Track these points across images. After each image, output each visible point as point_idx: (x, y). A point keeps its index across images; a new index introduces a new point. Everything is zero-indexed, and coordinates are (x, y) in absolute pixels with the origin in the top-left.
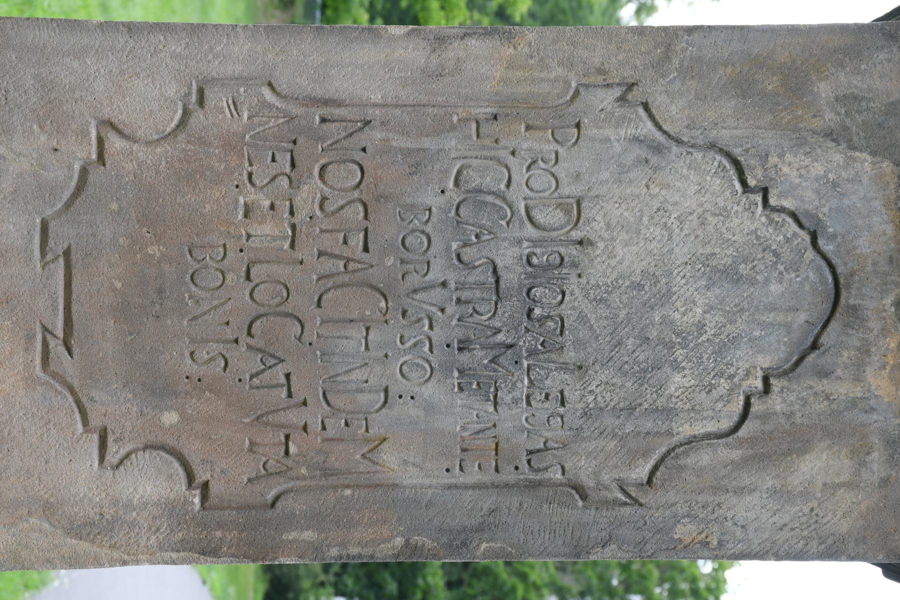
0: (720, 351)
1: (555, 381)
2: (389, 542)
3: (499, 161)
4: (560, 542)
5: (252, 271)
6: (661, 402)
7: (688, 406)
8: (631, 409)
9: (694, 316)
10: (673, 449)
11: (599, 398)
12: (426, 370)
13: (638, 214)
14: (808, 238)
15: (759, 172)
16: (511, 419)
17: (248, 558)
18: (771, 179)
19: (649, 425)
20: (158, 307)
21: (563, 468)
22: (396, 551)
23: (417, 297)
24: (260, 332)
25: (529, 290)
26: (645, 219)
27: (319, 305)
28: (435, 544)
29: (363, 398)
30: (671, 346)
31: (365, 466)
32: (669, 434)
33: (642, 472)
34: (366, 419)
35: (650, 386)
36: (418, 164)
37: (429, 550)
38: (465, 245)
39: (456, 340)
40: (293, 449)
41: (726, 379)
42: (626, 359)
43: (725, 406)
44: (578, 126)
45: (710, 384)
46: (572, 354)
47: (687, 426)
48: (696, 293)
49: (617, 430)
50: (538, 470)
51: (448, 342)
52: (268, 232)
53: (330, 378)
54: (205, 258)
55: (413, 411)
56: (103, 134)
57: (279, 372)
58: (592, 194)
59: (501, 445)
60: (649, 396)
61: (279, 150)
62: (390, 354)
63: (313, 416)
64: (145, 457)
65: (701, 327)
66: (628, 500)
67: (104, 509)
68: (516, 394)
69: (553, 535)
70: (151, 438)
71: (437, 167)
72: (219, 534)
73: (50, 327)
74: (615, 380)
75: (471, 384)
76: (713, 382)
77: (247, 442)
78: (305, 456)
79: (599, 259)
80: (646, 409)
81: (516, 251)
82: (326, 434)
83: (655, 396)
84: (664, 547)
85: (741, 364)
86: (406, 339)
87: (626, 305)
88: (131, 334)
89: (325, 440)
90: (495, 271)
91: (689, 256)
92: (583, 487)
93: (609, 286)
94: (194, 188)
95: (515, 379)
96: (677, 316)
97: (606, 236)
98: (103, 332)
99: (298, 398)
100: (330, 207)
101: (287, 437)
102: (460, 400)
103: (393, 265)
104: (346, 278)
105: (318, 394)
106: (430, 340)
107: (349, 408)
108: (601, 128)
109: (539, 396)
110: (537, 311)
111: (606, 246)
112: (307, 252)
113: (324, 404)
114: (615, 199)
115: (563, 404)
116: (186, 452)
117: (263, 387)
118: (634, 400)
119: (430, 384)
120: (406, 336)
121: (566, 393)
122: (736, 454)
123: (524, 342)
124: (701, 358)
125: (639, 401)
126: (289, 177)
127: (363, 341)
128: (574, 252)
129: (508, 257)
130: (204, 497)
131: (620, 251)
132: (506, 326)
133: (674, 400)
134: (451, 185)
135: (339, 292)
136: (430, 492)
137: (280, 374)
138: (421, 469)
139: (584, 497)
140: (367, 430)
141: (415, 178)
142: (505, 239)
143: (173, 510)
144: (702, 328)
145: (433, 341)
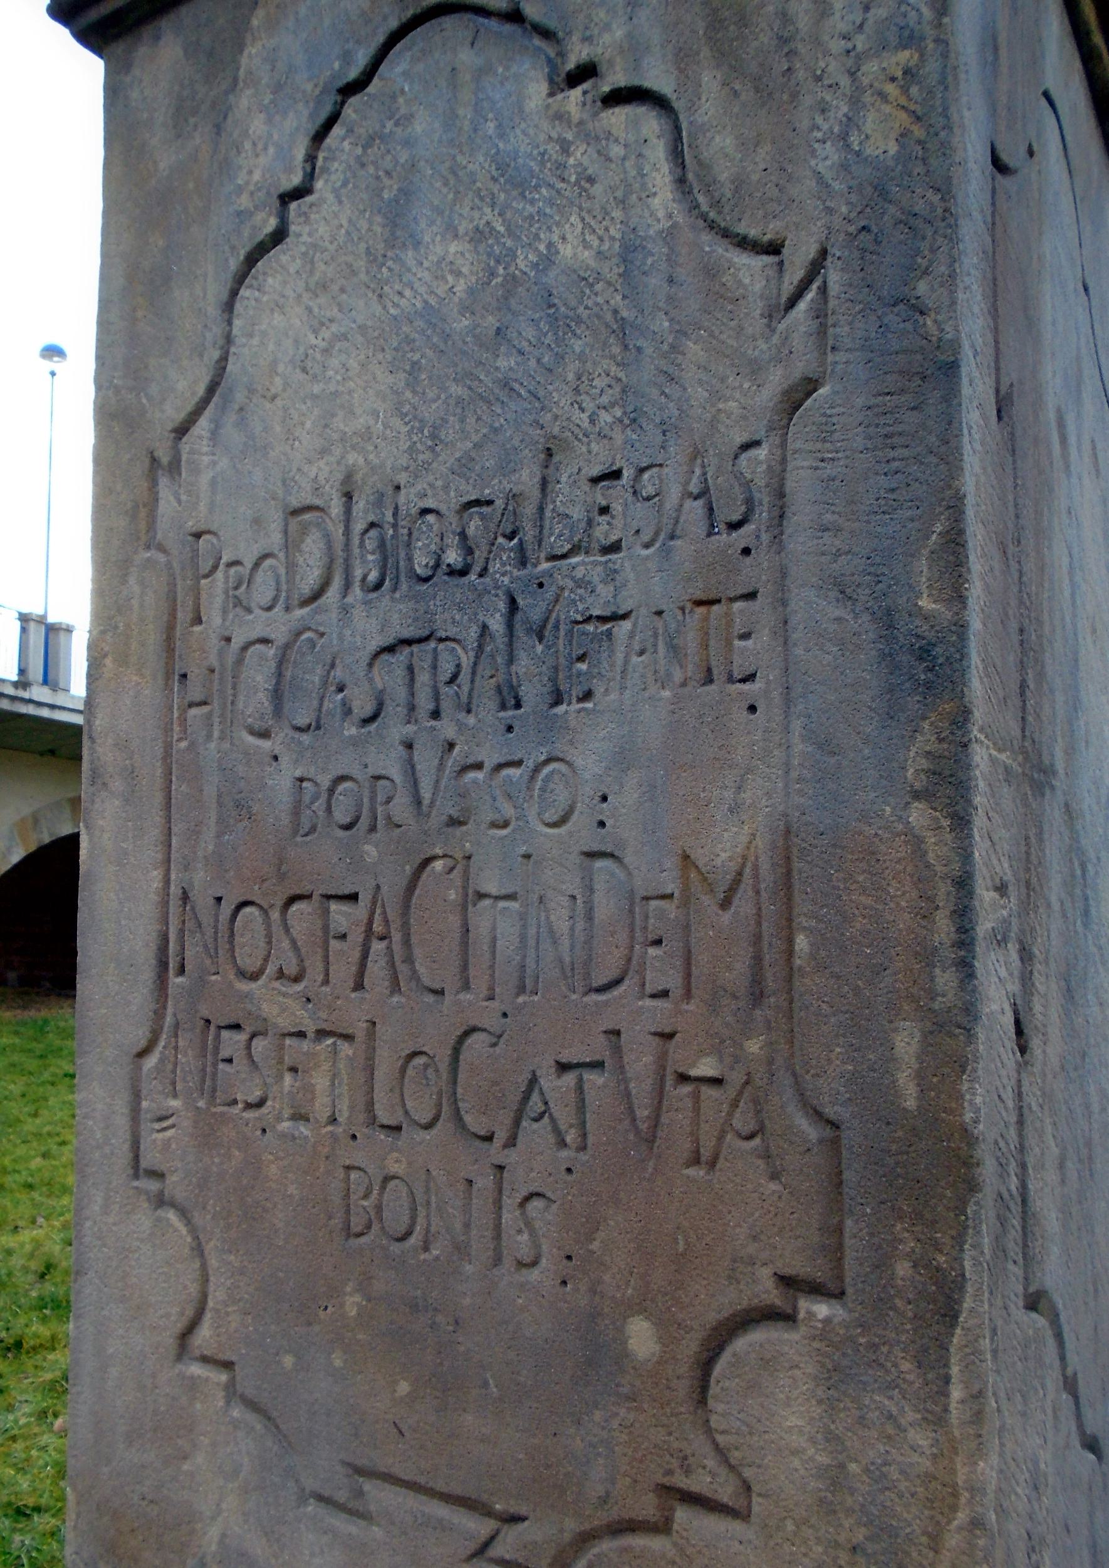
0: (521, 186)
1: (572, 498)
2: (920, 840)
3: (240, 661)
4: (912, 418)
5: (385, 1122)
6: (611, 271)
7: (617, 214)
8: (622, 329)
9: (462, 254)
10: (704, 217)
11: (605, 400)
12: (552, 772)
13: (309, 404)
14: (353, 101)
15: (259, 216)
16: (644, 581)
17: (965, 1203)
18: (268, 193)
19: (655, 281)
20: (440, 1318)
21: (746, 447)
22: (945, 823)
23: (426, 795)
24: (484, 1119)
25: (426, 580)
26: (317, 389)
27: (440, 993)
28: (926, 725)
29: (606, 907)
30: (512, 281)
31: (743, 904)
32: (670, 235)
33: (750, 269)
34: (647, 899)
35: (581, 302)
36: (238, 805)
37: (941, 740)
38: (348, 712)
39: (502, 714)
40: (706, 1068)
41: (569, 155)
42: (533, 363)
43: (616, 140)
44: (198, 536)
45: (577, 183)
46: (525, 474)
47: (656, 202)
48: (426, 264)
49: (665, 347)
50: (749, 502)
51: (503, 728)
52: (328, 1081)
53: (566, 978)
54: (364, 1208)
55: (628, 797)
56: (197, 1353)
57: (557, 1088)
58: (280, 493)
59: (700, 595)
60: (600, 300)
61: (216, 1049)
62: (523, 849)
63: (638, 1017)
64: (723, 1408)
65: (479, 235)
66: (814, 286)
67: (841, 1539)
68: (596, 575)
69: (895, 440)
70: (683, 1388)
71: (241, 769)
72: (903, 1269)
73: (473, 1546)
74: (571, 376)
75: (579, 674)
76: (573, 179)
77: (691, 1172)
78: (723, 1042)
79: (371, 457)
80: (624, 297)
81: (358, 613)
82: (677, 992)
83: (599, 287)
84: (920, 169)
85: (542, 137)
86: (497, 816)
87: (444, 389)
88: (486, 1384)
89: (688, 994)
90: (390, 649)
91: (370, 295)
92: (787, 393)
93: (413, 427)
94: (265, 1210)
95: (570, 584)
96: (461, 287)
97: (337, 451)
98: (482, 1441)
99: (599, 1048)
100: (291, 969)
101: (683, 1078)
102: (607, 697)
103: (376, 846)
104: (397, 937)
105: (596, 1003)
106: (500, 767)
107: (622, 937)
108: (198, 497)
109: (603, 532)
110: (453, 557)
111: (353, 447)
112: (354, 1013)
113: (616, 992)
114: (288, 448)
115: (616, 475)
116: (713, 1317)
117: (583, 1124)
118: (607, 326)
119: (579, 762)
120: (490, 816)
121: (596, 471)
122: (710, 80)
123: (503, 574)
124: (531, 217)
125: (609, 317)
126: (253, 1036)
127: (502, 904)
128: (361, 504)
129: (370, 623)
130: (816, 1290)
131: (361, 422)
132: (476, 614)
133: (605, 247)
134: (266, 744)
135: (418, 952)
136: (799, 747)
137: (559, 1083)
138: (749, 770)
139: (810, 385)
140: (670, 896)
141: (255, 810)
142: (341, 637)
143: (841, 1371)
144: (481, 233)
145: (502, 760)
